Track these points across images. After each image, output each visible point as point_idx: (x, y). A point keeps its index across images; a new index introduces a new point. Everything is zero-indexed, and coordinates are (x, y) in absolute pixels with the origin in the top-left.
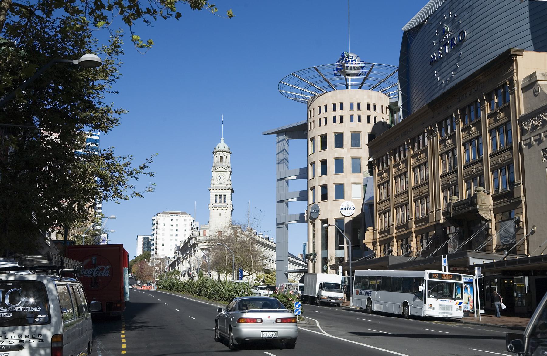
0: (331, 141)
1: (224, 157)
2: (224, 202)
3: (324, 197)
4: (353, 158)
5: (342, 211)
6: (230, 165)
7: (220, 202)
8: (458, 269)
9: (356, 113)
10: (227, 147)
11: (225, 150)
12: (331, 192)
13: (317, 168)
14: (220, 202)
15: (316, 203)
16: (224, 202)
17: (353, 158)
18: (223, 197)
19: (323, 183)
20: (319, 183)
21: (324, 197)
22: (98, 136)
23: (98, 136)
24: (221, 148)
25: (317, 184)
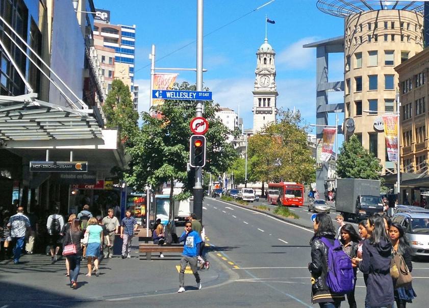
0: (366, 83)
1: (268, 59)
2: (269, 105)
3: (359, 112)
4: (385, 75)
5: (375, 126)
6: (274, 67)
7: (264, 105)
8: (422, 55)
9: (389, 31)
10: (270, 48)
11: (269, 51)
12: (366, 107)
13: (353, 84)
14: (264, 105)
15: (351, 117)
16: (269, 105)
17: (385, 75)
18: (267, 101)
19: (358, 99)
20: (355, 99)
21: (359, 112)
22: (133, 29)
23: (133, 29)
24: (265, 50)
25: (353, 100)
